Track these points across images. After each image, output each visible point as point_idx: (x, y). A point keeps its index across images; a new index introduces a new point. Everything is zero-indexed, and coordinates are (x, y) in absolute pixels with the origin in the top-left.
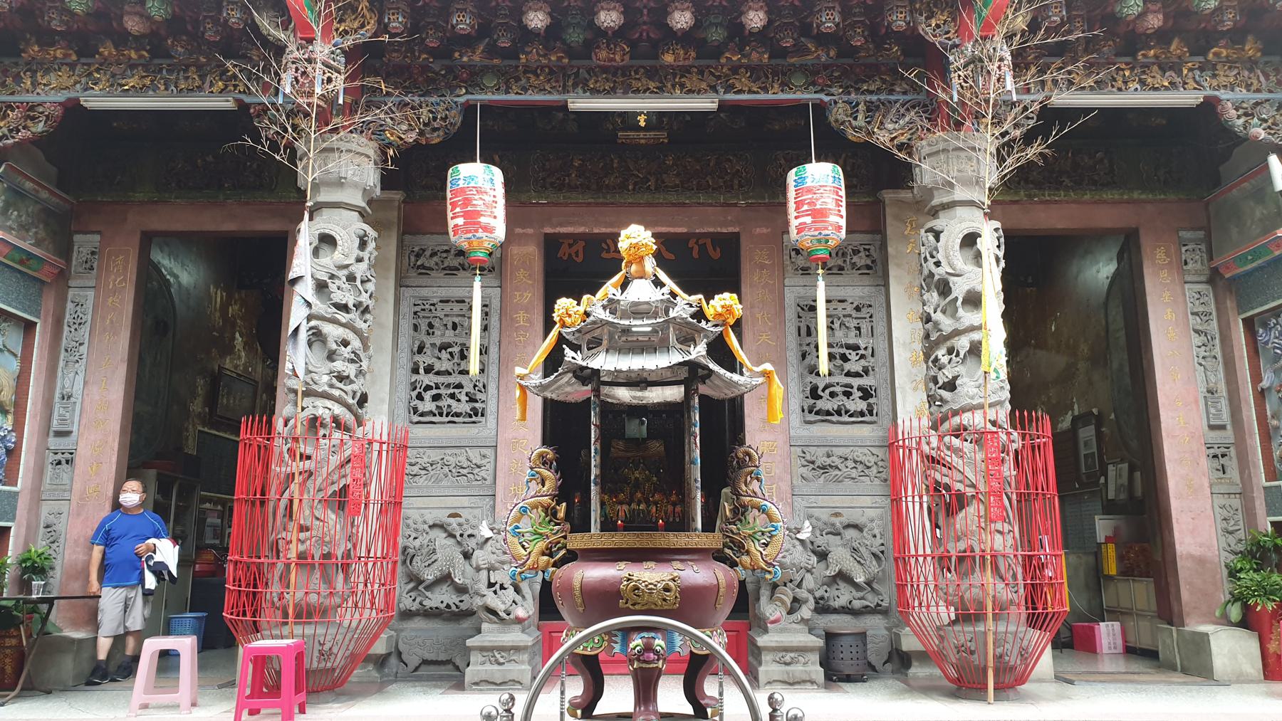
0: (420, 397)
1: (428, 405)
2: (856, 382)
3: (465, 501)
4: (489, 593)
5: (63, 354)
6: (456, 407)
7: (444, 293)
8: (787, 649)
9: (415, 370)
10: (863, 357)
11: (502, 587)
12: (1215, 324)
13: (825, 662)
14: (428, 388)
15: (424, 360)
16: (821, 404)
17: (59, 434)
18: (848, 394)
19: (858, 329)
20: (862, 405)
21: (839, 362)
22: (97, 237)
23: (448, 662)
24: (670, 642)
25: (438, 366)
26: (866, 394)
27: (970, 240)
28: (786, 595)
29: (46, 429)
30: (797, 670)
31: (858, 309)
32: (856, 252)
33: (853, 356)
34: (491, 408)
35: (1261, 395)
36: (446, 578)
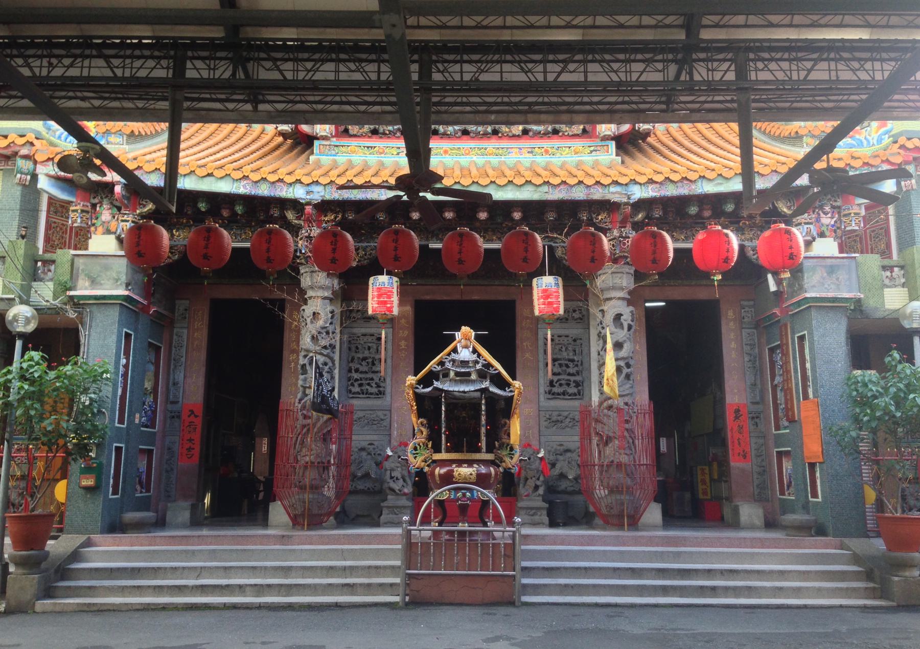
0: (352, 385)
1: (356, 389)
2: (572, 378)
3: (375, 437)
4: (391, 481)
5: (173, 362)
6: (371, 390)
7: (363, 331)
8: (532, 509)
9: (350, 371)
10: (577, 365)
11: (397, 479)
12: (757, 350)
13: (549, 514)
14: (356, 380)
15: (354, 366)
16: (555, 390)
17: (172, 403)
18: (568, 385)
19: (575, 351)
20: (575, 390)
21: (564, 368)
22: (188, 302)
23: (368, 516)
24: (472, 495)
25: (361, 369)
26: (577, 384)
27: (618, 317)
28: (531, 483)
29: (167, 400)
30: (537, 518)
31: (575, 340)
32: (574, 311)
33: (571, 365)
34: (388, 390)
35: (774, 388)
36: (367, 476)
